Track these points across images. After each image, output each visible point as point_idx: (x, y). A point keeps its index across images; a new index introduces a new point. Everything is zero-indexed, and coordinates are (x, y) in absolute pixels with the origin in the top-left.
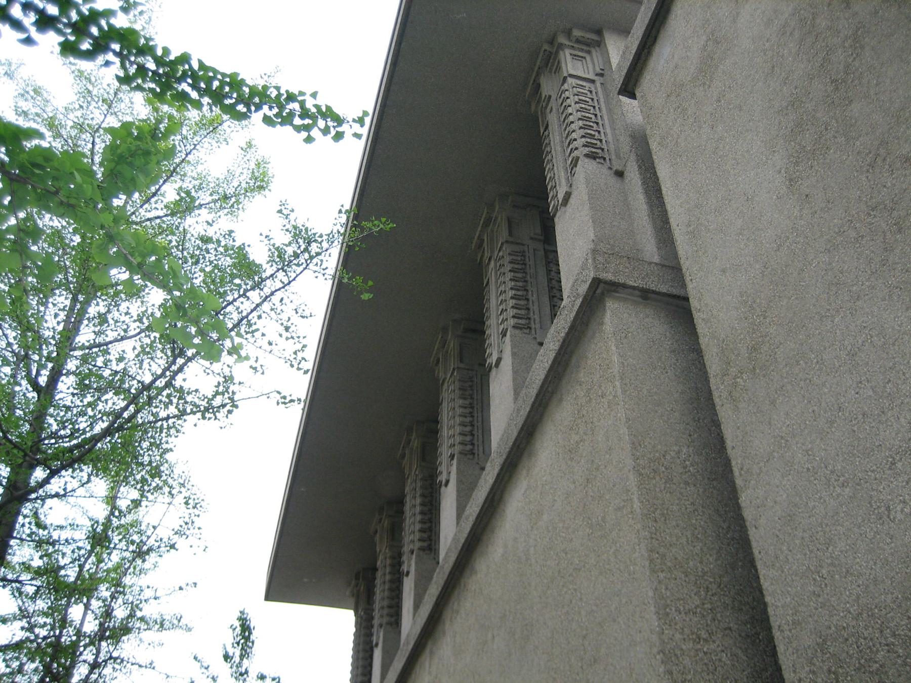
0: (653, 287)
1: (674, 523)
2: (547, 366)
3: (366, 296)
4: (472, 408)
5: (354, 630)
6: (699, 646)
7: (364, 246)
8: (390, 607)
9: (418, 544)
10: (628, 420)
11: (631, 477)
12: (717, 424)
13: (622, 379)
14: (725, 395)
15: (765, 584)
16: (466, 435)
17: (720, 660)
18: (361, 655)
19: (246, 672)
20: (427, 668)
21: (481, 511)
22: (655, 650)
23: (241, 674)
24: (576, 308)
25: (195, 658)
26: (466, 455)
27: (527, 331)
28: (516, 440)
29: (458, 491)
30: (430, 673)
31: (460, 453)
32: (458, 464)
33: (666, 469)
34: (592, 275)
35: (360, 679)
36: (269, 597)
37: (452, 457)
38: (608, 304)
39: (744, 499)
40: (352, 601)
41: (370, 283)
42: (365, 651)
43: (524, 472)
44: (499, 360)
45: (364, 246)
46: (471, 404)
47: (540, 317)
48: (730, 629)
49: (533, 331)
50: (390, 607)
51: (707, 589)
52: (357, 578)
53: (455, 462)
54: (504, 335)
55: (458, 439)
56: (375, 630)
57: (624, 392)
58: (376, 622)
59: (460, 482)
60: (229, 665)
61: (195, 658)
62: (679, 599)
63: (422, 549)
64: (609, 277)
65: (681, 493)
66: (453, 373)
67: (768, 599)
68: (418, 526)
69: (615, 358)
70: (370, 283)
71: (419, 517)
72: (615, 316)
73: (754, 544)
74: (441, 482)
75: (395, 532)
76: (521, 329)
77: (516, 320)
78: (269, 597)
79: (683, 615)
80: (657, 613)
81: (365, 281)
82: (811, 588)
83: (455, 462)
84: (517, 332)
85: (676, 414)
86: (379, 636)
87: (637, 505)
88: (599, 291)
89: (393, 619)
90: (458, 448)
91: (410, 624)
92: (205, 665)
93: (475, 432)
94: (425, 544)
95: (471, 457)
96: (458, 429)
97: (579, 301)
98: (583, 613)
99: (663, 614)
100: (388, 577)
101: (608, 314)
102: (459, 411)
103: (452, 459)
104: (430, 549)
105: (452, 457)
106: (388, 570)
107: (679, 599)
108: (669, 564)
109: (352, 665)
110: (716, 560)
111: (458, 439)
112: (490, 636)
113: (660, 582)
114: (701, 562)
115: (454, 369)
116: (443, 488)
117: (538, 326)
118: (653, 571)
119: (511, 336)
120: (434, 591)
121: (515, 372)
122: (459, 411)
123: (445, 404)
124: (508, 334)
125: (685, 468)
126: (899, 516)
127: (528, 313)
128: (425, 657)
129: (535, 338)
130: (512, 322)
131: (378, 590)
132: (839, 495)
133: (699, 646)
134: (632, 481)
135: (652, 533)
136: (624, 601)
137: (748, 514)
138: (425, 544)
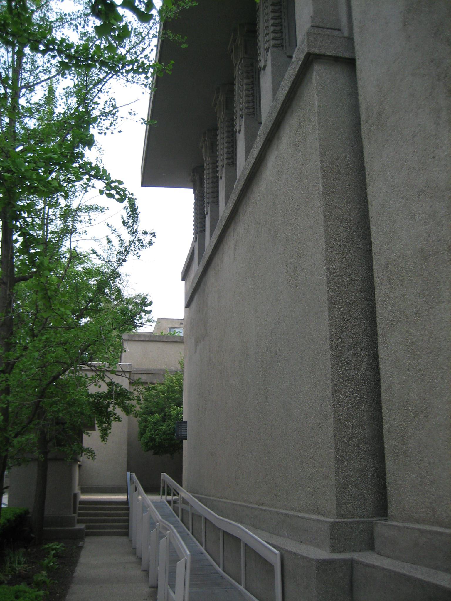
0: (341, 54)
1: (338, 196)
2: (285, 93)
3: (184, 46)
4: (253, 84)
5: (194, 201)
6: (343, 256)
7: (180, 17)
8: (213, 192)
9: (226, 162)
10: (320, 140)
11: (320, 172)
12: (362, 147)
13: (318, 115)
14: (366, 133)
15: (372, 233)
16: (249, 103)
17: (353, 262)
18: (199, 216)
19: (136, 231)
20: (232, 234)
21: (255, 162)
22: (324, 258)
23: (134, 233)
24: (299, 66)
25: (108, 225)
26: (250, 115)
27: (281, 48)
28: (271, 129)
29: (245, 138)
30: (234, 239)
31: (246, 114)
32: (246, 119)
33: (337, 167)
34: (306, 51)
35: (199, 230)
36: (143, 185)
37: (242, 116)
38: (315, 68)
39: (369, 190)
40: (192, 184)
41: (186, 38)
42: (201, 218)
43: (276, 147)
44: (265, 66)
45: (180, 17)
46: (252, 82)
47: (289, 38)
48: (359, 247)
49: (284, 48)
50: (213, 192)
51: (351, 229)
52: (194, 172)
53: (243, 119)
54: (268, 51)
55: (245, 105)
56: (205, 205)
57: (319, 123)
58: (206, 201)
59: (246, 132)
60: (126, 227)
61: (108, 225)
62: (336, 235)
63: (228, 164)
64: (316, 51)
65: (344, 180)
66: (241, 61)
67: (372, 240)
68: (226, 151)
69: (316, 102)
70: (186, 38)
71: (226, 145)
72: (319, 74)
73: (370, 213)
74: (236, 130)
75: (213, 147)
76: (277, 47)
77: (274, 41)
78: (143, 185)
79: (338, 242)
80: (325, 242)
81: (183, 37)
82: (386, 240)
83: (243, 119)
84: (275, 49)
85: (346, 134)
86: (208, 209)
87: (321, 187)
88: (310, 58)
89: (215, 195)
90: (245, 111)
91: (224, 209)
92: (113, 228)
93: (255, 100)
94: (230, 161)
95: (253, 116)
96: (245, 99)
97: (300, 63)
98: (299, 232)
99: (328, 242)
100: (211, 176)
101: (315, 73)
102: (245, 87)
103: (242, 117)
104: (233, 164)
105: (242, 116)
106: (211, 171)
107: (336, 235)
108: (334, 217)
109: (195, 208)
110: (357, 214)
111: (245, 105)
112: (260, 229)
113: (328, 227)
114: (350, 216)
115: (241, 59)
116: (237, 134)
117: (287, 44)
118: (326, 222)
119: (271, 53)
120: (234, 197)
121: (273, 77)
122: (245, 87)
123: (237, 80)
124: (270, 51)
125: (347, 165)
126: (417, 220)
127: (282, 36)
128: (231, 230)
129: (286, 53)
130: (272, 43)
131: (205, 182)
132: (400, 202)
133: (343, 256)
134: (319, 174)
135: (326, 202)
136: (314, 232)
137: (369, 198)
138: (230, 161)
